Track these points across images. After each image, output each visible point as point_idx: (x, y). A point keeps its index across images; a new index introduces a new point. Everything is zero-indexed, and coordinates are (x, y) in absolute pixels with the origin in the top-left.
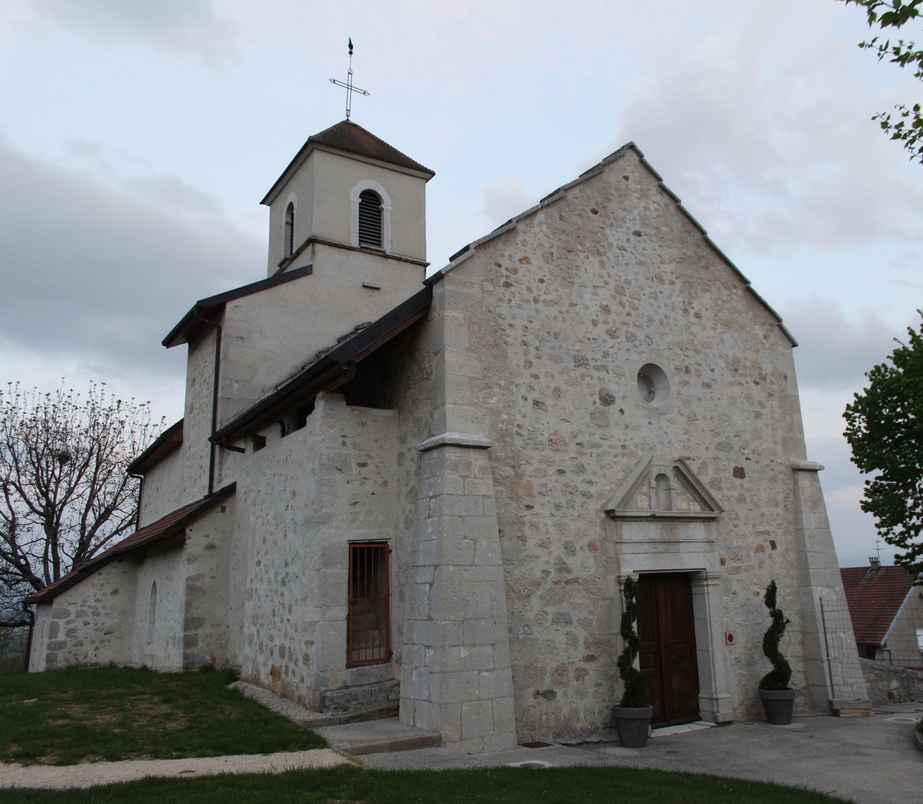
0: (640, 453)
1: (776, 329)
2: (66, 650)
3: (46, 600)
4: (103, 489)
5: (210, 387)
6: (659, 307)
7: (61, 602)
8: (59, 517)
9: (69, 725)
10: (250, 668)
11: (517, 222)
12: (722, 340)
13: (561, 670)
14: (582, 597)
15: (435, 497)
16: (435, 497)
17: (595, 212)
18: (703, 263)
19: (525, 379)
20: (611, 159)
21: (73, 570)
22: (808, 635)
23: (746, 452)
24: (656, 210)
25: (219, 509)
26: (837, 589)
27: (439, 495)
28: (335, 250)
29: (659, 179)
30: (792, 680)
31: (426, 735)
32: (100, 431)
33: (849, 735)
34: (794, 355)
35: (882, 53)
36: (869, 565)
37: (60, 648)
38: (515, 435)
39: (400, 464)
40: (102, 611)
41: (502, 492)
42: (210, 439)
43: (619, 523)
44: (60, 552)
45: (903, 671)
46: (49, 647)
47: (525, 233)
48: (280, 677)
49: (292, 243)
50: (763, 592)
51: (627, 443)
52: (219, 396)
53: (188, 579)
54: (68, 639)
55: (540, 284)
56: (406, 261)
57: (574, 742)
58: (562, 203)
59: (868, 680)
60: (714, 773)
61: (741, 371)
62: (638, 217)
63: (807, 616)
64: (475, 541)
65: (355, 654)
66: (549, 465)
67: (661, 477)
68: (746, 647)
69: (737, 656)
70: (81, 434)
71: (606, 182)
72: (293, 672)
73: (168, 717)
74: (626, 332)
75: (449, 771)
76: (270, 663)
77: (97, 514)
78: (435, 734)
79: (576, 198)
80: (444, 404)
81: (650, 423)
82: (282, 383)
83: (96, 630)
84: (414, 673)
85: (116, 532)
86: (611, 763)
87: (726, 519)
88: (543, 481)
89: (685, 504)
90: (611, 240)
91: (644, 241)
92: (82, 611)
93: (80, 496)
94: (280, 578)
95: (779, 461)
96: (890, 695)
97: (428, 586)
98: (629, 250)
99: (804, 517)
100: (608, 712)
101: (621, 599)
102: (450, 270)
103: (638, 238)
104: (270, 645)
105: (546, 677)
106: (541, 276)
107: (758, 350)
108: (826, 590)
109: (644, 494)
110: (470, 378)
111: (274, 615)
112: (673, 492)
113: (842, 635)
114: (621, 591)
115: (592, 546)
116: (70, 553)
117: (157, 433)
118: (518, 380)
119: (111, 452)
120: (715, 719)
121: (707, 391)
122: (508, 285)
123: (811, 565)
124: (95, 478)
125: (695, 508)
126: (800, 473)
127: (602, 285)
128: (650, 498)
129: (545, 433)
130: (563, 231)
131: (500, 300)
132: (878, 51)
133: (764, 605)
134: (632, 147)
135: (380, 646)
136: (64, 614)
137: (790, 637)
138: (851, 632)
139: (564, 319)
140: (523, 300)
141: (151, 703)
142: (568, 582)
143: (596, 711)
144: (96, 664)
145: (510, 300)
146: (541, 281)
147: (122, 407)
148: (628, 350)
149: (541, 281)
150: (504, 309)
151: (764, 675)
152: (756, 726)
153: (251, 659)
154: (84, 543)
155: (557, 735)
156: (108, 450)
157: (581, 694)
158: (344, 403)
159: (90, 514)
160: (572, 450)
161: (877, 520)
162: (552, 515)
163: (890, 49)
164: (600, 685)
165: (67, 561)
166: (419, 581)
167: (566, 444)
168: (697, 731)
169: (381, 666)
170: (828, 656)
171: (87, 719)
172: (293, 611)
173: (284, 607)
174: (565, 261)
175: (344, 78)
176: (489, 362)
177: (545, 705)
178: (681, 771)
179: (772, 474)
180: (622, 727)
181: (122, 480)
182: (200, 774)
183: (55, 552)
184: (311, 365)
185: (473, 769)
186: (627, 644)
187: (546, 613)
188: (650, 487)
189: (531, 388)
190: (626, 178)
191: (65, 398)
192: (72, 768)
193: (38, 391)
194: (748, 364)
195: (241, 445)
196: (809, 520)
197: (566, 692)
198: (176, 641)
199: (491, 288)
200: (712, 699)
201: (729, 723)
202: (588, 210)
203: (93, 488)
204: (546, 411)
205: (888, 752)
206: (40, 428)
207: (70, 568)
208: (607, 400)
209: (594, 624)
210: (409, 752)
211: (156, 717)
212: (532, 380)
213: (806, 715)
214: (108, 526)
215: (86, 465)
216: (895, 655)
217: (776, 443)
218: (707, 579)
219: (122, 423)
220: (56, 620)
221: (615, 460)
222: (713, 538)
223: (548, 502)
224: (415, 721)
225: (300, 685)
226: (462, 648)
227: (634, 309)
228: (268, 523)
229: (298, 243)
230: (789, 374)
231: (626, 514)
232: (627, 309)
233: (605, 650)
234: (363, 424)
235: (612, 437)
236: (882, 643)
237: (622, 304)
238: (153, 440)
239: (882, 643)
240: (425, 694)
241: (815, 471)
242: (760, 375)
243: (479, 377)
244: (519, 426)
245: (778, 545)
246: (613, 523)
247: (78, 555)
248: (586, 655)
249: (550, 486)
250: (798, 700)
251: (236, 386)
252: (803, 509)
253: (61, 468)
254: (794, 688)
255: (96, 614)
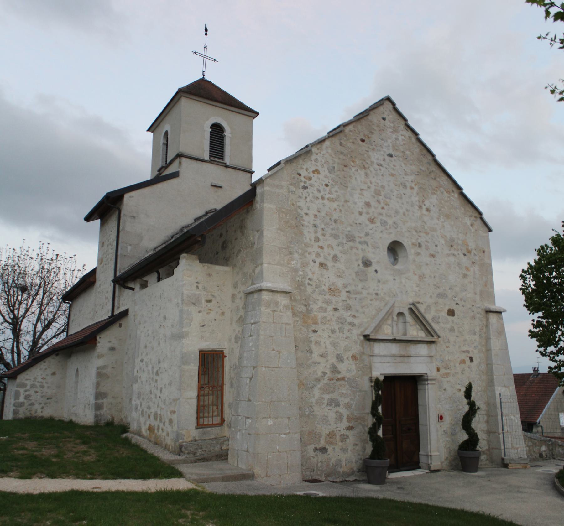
0: (387, 298)
1: (479, 221)
2: (24, 407)
3: (13, 377)
4: (47, 309)
5: (113, 248)
6: (403, 204)
7: (21, 378)
8: (20, 325)
9: (26, 454)
10: (135, 425)
11: (312, 146)
12: (444, 226)
13: (331, 435)
14: (347, 390)
15: (254, 323)
16: (254, 323)
17: (363, 141)
18: (433, 175)
19: (315, 249)
20: (374, 106)
21: (29, 358)
22: (491, 417)
23: (456, 299)
24: (403, 140)
25: (118, 325)
26: (511, 388)
27: (257, 323)
28: (194, 162)
29: (405, 120)
30: (479, 444)
31: (245, 472)
32: (45, 273)
33: (513, 480)
34: (490, 237)
35: (552, 43)
36: (532, 372)
37: (21, 406)
38: (307, 285)
39: (233, 302)
40: (46, 385)
41: (298, 321)
42: (113, 281)
43: (372, 343)
44: (21, 347)
45: (550, 440)
46: (14, 405)
47: (317, 154)
48: (154, 432)
49: (166, 157)
50: (464, 389)
51: (379, 292)
52: (119, 253)
53: (98, 368)
54: (25, 401)
55: (326, 187)
56: (240, 170)
57: (338, 480)
58: (341, 135)
59: (527, 446)
60: (427, 502)
61: (455, 247)
62: (391, 145)
63: (491, 405)
64: (280, 352)
65: (201, 420)
66: (328, 305)
67: (400, 314)
68: (451, 424)
69: (445, 429)
70: (34, 275)
71: (371, 121)
72: (162, 429)
73: (85, 453)
74: (381, 220)
75: (259, 496)
76: (148, 423)
77: (43, 324)
78: (250, 472)
79: (351, 131)
80: (262, 264)
81: (394, 279)
82: (159, 246)
83: (42, 396)
84: (238, 433)
85: (55, 336)
86: (362, 494)
87: (442, 342)
88: (323, 314)
89: (415, 332)
90: (373, 159)
91: (395, 160)
92: (34, 385)
93: (33, 313)
94: (155, 371)
95: (478, 306)
96: (541, 455)
97: (249, 380)
98: (384, 166)
99: (492, 342)
100: (361, 462)
101: (372, 391)
102: (267, 177)
103: (391, 158)
104: (148, 412)
105: (322, 439)
106: (327, 183)
107: (467, 233)
108: (504, 389)
109: (389, 325)
110: (279, 248)
111: (151, 393)
112: (408, 324)
113: (512, 417)
114: (372, 386)
115: (354, 357)
116: (27, 348)
117: (80, 275)
118: (310, 250)
119: (52, 286)
120: (429, 468)
121: (432, 259)
122: (305, 188)
123: (495, 373)
124: (42, 302)
125: (422, 335)
126: (491, 314)
127: (366, 188)
128: (393, 328)
129: (326, 284)
130: (342, 153)
131: (300, 197)
132: (550, 41)
133: (464, 397)
134: (388, 99)
135: (217, 416)
136: (23, 385)
137: (479, 418)
138: (518, 416)
139: (341, 211)
140: (314, 197)
141: (75, 444)
142: (338, 380)
143: (354, 461)
144: (42, 417)
145: (306, 198)
146: (327, 185)
147: (59, 259)
148: (382, 232)
149: (327, 185)
150: (302, 203)
151: (462, 441)
152: (455, 473)
153: (138, 421)
154: (35, 342)
155: (328, 476)
156: (50, 285)
157: (344, 450)
158: (198, 261)
159: (39, 325)
160: (344, 295)
161: (538, 343)
162: (329, 337)
163: (557, 40)
164: (357, 445)
165: (25, 353)
166: (243, 376)
167: (340, 292)
168: (417, 475)
169: (218, 428)
170: (503, 430)
171: (37, 451)
172: (163, 391)
173: (157, 389)
174: (343, 172)
175: (201, 51)
176: (292, 237)
177: (321, 457)
178: (406, 501)
179: (472, 314)
180: (370, 471)
181: (58, 304)
182: (104, 490)
183: (18, 347)
184: (178, 236)
185: (274, 496)
186: (374, 420)
187: (323, 399)
188: (393, 321)
189: (318, 255)
190: (384, 119)
191: (25, 252)
192: (28, 481)
193: (9, 247)
194: (460, 242)
195: (131, 285)
196: (495, 344)
197: (334, 449)
198: (90, 406)
199: (294, 189)
200: (427, 456)
201: (438, 471)
202: (358, 139)
203: (40, 308)
204: (328, 269)
205: (537, 491)
206: (10, 270)
207: (27, 357)
208: (367, 263)
209: (353, 407)
210: (234, 482)
211: (78, 453)
212: (320, 250)
213: (487, 466)
214: (50, 333)
215: (37, 294)
216: (544, 430)
217: (475, 294)
218: (427, 380)
219: (59, 268)
220: (18, 389)
221: (370, 302)
222: (432, 354)
223: (327, 328)
224: (238, 463)
225: (167, 437)
226: (269, 419)
227: (386, 205)
228: (148, 335)
229: (170, 157)
230: (486, 250)
231: (377, 338)
232: (382, 205)
233: (360, 423)
234: (210, 275)
235: (369, 287)
236: (538, 421)
237: (378, 202)
238: (78, 280)
239: (538, 421)
240: (245, 447)
241: (500, 313)
242: (467, 249)
243: (284, 247)
244: (310, 279)
245: (474, 360)
246: (368, 343)
247: (31, 350)
248: (348, 426)
249: (328, 318)
250: (483, 457)
251: (129, 248)
252: (492, 337)
253: (22, 295)
254: (480, 450)
255: (42, 387)
